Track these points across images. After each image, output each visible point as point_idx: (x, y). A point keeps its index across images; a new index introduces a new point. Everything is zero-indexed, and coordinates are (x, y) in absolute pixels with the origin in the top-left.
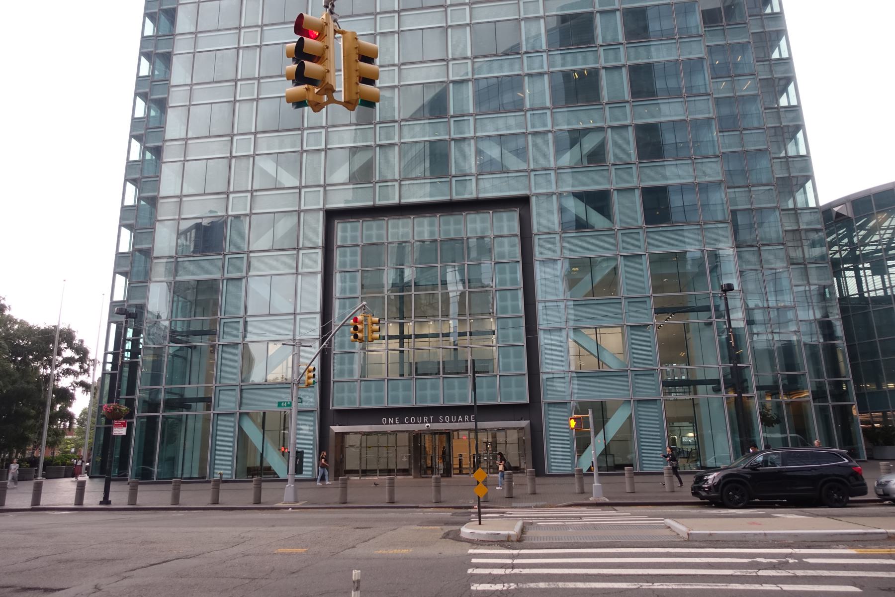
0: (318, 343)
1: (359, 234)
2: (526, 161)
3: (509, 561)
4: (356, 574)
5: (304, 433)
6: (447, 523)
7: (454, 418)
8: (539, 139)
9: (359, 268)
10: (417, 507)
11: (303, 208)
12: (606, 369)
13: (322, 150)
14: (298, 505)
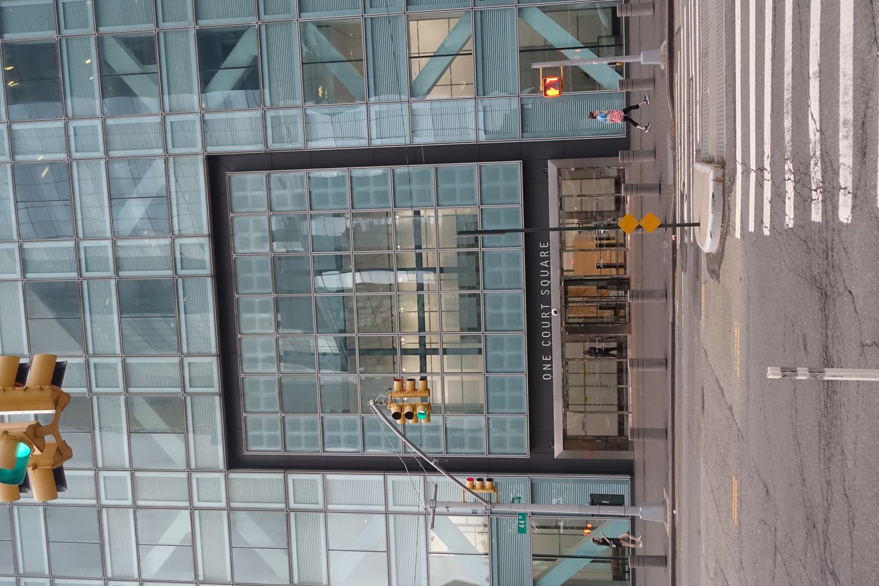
0: (433, 478)
1: (264, 418)
2: (151, 159)
3: (753, 176)
4: (773, 374)
5: (565, 495)
6: (697, 277)
7: (543, 273)
8: (115, 138)
9: (316, 417)
10: (673, 324)
11: (223, 504)
12: (470, 46)
13: (132, 476)
14: (669, 501)
